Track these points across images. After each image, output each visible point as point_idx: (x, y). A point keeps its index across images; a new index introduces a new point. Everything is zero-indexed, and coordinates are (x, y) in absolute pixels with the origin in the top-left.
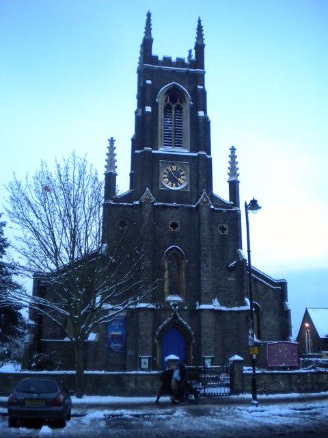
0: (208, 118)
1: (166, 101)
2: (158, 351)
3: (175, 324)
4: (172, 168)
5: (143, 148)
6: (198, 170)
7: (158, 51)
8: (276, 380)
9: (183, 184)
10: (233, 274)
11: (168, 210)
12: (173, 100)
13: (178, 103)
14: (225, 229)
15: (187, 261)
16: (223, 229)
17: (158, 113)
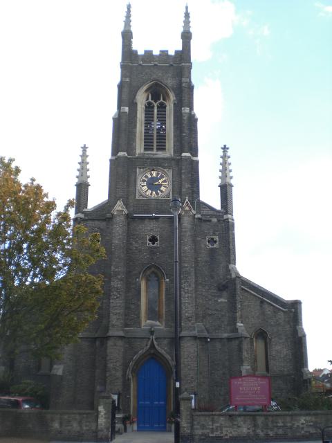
0: (194, 115)
1: (147, 99)
2: (132, 385)
3: (153, 356)
4: (151, 174)
6: (180, 174)
7: (139, 47)
8: (235, 423)
9: (166, 188)
10: (225, 293)
11: (146, 222)
12: (156, 97)
13: (162, 100)
14: (215, 242)
15: (168, 280)
16: (212, 241)
17: (136, 113)
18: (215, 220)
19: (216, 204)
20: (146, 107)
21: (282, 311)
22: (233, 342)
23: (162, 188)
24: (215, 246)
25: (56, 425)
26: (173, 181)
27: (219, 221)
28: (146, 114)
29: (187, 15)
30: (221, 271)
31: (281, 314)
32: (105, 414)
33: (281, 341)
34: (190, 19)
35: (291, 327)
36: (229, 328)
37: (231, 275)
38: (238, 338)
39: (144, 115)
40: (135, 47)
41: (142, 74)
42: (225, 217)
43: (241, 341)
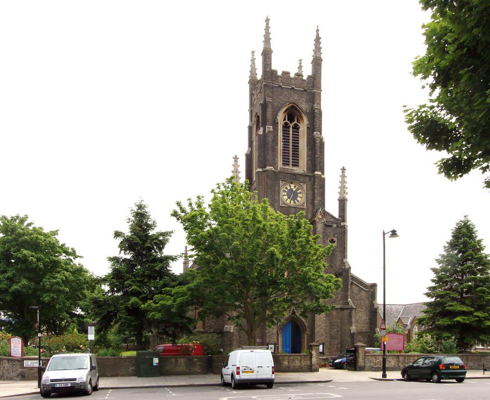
1: (284, 120)
7: (279, 65)
12: (291, 118)
13: (296, 122)
14: (334, 242)
18: (335, 226)
19: (335, 213)
20: (283, 126)
22: (345, 311)
23: (299, 199)
25: (286, 363)
27: (337, 226)
29: (318, 40)
30: (338, 263)
31: (363, 293)
32: (316, 355)
33: (362, 310)
34: (321, 45)
35: (369, 301)
36: (341, 302)
37: (345, 266)
40: (274, 67)
41: (281, 95)
42: (342, 224)
43: (351, 312)
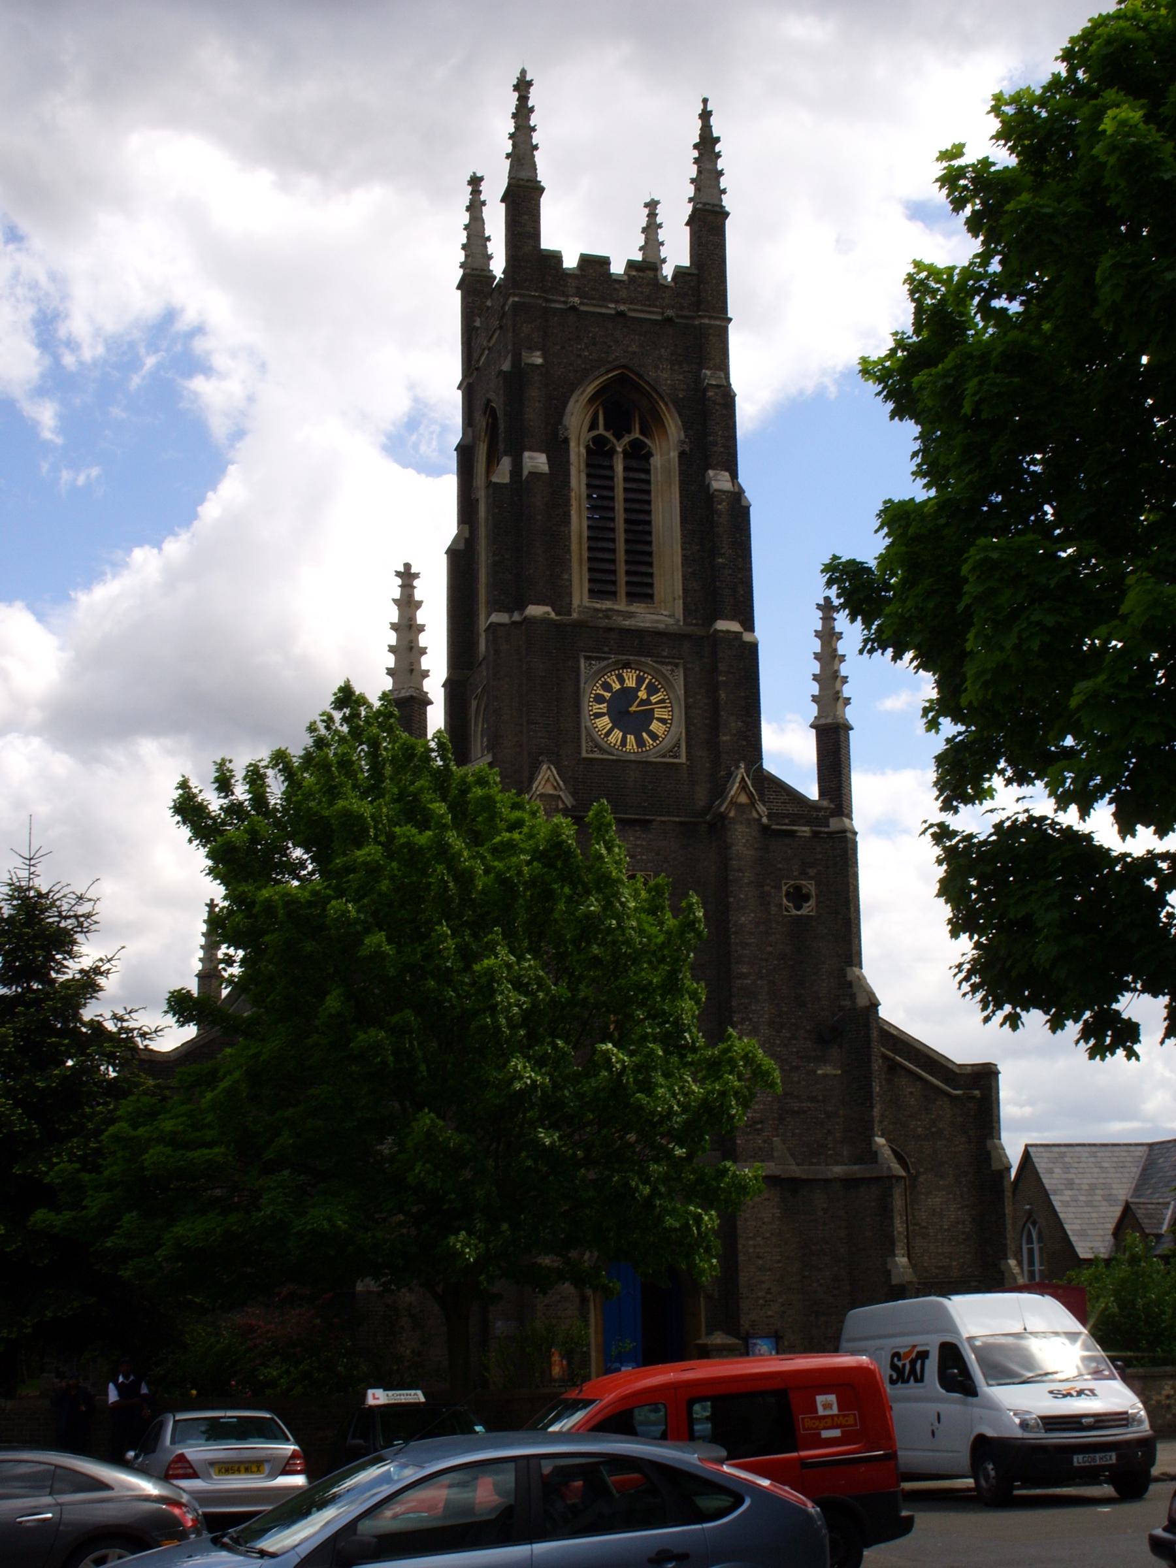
1: (593, 426)
4: (621, 680)
5: (521, 607)
12: (617, 423)
13: (636, 434)
14: (806, 898)
18: (805, 830)
21: (949, 1095)
24: (803, 912)
26: (688, 707)
28: (589, 476)
38: (877, 1179)
39: (583, 476)
